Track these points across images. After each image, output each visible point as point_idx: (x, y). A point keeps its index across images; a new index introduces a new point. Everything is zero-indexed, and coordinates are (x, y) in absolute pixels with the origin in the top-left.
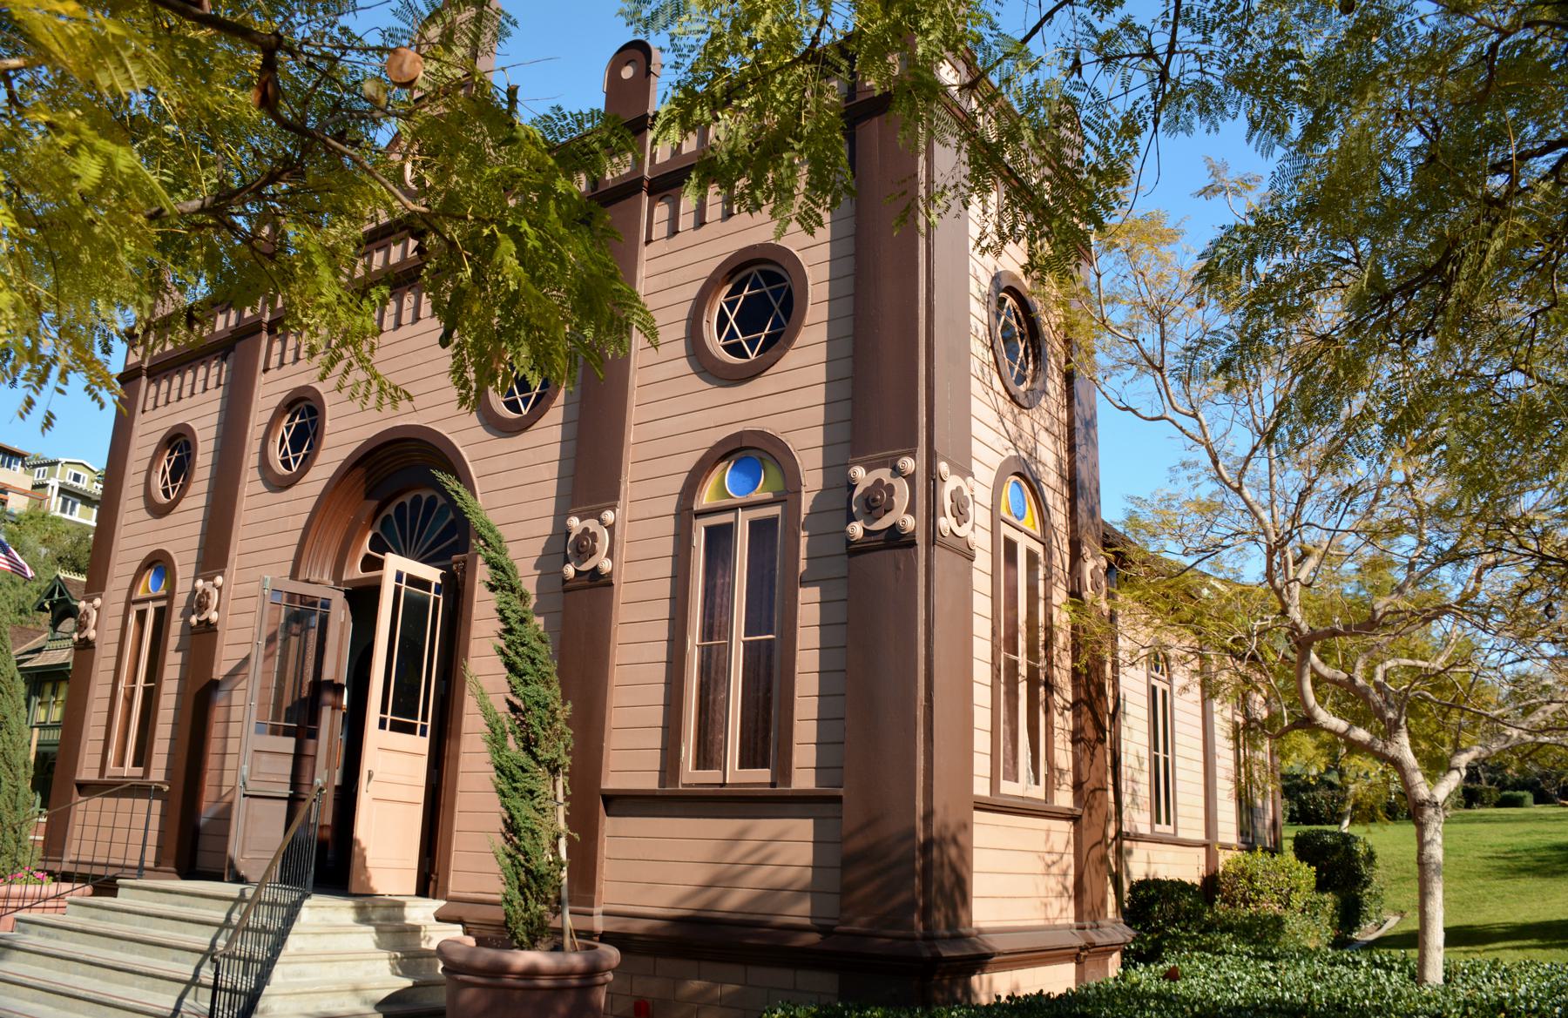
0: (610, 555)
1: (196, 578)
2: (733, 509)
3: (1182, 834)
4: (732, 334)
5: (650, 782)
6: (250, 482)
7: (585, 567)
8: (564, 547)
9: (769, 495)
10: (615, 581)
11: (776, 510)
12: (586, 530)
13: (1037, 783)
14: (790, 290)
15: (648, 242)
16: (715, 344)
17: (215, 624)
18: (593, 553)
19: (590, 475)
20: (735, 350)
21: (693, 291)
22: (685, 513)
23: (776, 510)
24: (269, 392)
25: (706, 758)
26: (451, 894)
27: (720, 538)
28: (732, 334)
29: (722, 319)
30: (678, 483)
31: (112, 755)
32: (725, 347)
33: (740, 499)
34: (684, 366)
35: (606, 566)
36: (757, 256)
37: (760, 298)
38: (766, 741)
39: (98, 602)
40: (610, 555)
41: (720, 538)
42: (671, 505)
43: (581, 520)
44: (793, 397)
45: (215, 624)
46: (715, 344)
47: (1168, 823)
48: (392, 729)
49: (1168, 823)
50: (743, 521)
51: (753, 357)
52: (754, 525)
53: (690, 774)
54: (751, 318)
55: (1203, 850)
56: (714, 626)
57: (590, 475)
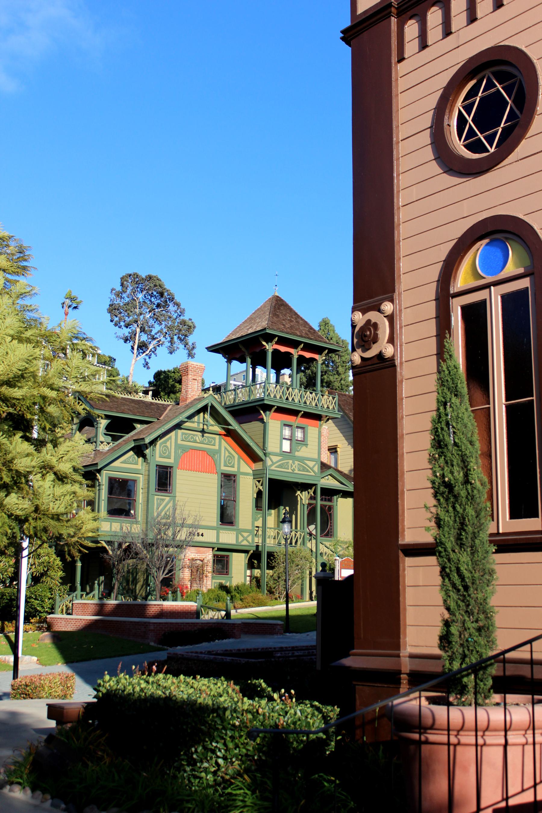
0: (391, 340)
1: (354, 310)
2: (487, 286)
4: (471, 133)
7: (369, 354)
8: (364, 337)
9: (521, 270)
10: (397, 362)
11: (525, 283)
12: (369, 321)
13: (493, 520)
14: (520, 81)
15: (401, 59)
16: (458, 146)
17: (392, 359)
18: (375, 340)
21: (433, 101)
22: (444, 296)
23: (525, 283)
27: (475, 316)
28: (471, 133)
29: (462, 121)
30: (435, 272)
32: (466, 146)
33: (490, 279)
34: (435, 168)
35: (389, 351)
36: (484, 60)
39: (387, 307)
40: (391, 340)
41: (475, 316)
42: (431, 291)
43: (363, 314)
45: (392, 359)
46: (458, 146)
51: (492, 150)
52: (505, 298)
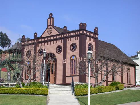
3: (131, 84)
5: (69, 76)
6: (37, 56)
19: (65, 57)
20: (73, 49)
22: (70, 59)
24: (38, 48)
25: (72, 74)
26: (57, 83)
27: (72, 61)
31: (26, 77)
37: (74, 46)
38: (75, 73)
41: (72, 61)
44: (77, 52)
47: (115, 80)
48: (63, 64)
49: (115, 80)
50: (73, 60)
53: (71, 75)
54: (74, 47)
55: (108, 80)
56: (72, 66)
57: (65, 57)
